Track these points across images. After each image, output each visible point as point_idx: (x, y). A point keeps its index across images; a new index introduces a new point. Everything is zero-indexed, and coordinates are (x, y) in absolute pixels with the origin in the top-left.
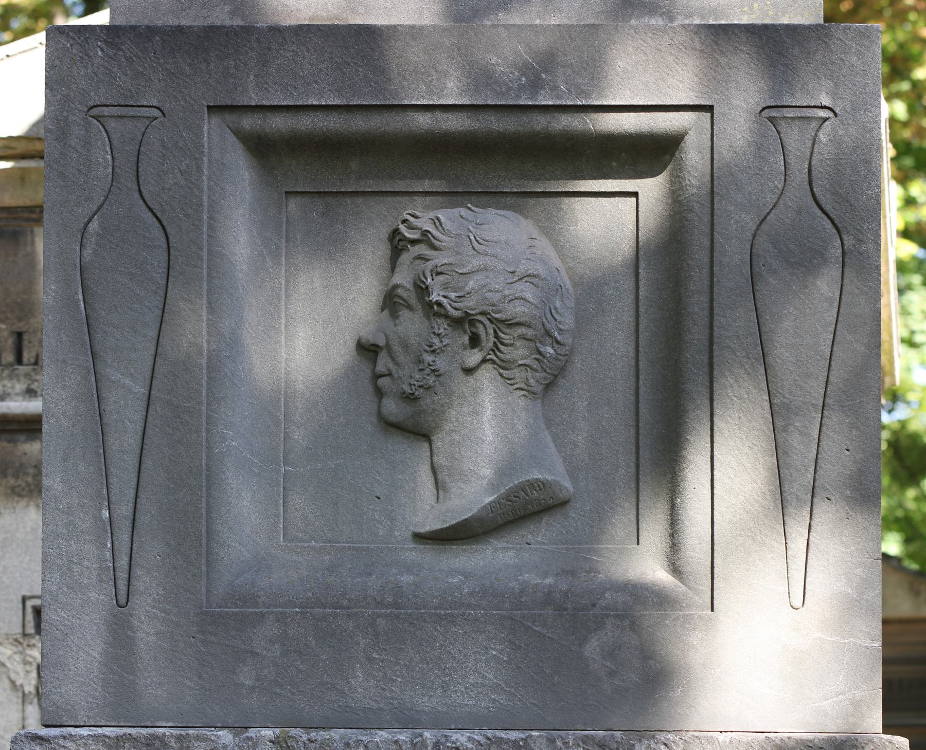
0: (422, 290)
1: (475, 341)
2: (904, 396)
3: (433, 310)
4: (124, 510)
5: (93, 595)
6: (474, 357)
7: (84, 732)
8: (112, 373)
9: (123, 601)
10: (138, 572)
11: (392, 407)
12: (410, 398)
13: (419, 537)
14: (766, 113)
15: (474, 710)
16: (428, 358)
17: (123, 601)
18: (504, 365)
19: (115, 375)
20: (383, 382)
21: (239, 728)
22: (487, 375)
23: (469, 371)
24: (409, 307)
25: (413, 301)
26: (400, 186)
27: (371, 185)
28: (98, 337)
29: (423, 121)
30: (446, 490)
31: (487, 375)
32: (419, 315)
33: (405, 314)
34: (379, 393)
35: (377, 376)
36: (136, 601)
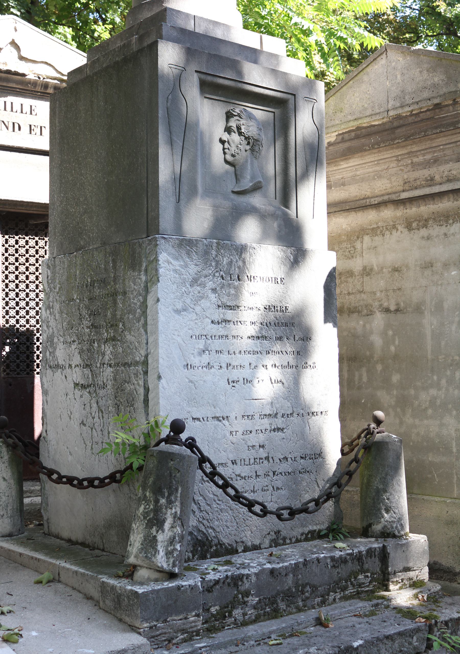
0: (239, 128)
5: (171, 199)
7: (174, 237)
8: (175, 138)
10: (181, 194)
12: (233, 156)
13: (233, 192)
14: (170, 66)
15: (57, 306)
16: (240, 146)
19: (175, 139)
20: (226, 150)
24: (235, 132)
25: (236, 130)
26: (234, 101)
27: (234, 101)
28: (171, 128)
30: (239, 181)
32: (237, 134)
33: (233, 133)
34: (225, 153)
35: (224, 149)
36: (181, 202)
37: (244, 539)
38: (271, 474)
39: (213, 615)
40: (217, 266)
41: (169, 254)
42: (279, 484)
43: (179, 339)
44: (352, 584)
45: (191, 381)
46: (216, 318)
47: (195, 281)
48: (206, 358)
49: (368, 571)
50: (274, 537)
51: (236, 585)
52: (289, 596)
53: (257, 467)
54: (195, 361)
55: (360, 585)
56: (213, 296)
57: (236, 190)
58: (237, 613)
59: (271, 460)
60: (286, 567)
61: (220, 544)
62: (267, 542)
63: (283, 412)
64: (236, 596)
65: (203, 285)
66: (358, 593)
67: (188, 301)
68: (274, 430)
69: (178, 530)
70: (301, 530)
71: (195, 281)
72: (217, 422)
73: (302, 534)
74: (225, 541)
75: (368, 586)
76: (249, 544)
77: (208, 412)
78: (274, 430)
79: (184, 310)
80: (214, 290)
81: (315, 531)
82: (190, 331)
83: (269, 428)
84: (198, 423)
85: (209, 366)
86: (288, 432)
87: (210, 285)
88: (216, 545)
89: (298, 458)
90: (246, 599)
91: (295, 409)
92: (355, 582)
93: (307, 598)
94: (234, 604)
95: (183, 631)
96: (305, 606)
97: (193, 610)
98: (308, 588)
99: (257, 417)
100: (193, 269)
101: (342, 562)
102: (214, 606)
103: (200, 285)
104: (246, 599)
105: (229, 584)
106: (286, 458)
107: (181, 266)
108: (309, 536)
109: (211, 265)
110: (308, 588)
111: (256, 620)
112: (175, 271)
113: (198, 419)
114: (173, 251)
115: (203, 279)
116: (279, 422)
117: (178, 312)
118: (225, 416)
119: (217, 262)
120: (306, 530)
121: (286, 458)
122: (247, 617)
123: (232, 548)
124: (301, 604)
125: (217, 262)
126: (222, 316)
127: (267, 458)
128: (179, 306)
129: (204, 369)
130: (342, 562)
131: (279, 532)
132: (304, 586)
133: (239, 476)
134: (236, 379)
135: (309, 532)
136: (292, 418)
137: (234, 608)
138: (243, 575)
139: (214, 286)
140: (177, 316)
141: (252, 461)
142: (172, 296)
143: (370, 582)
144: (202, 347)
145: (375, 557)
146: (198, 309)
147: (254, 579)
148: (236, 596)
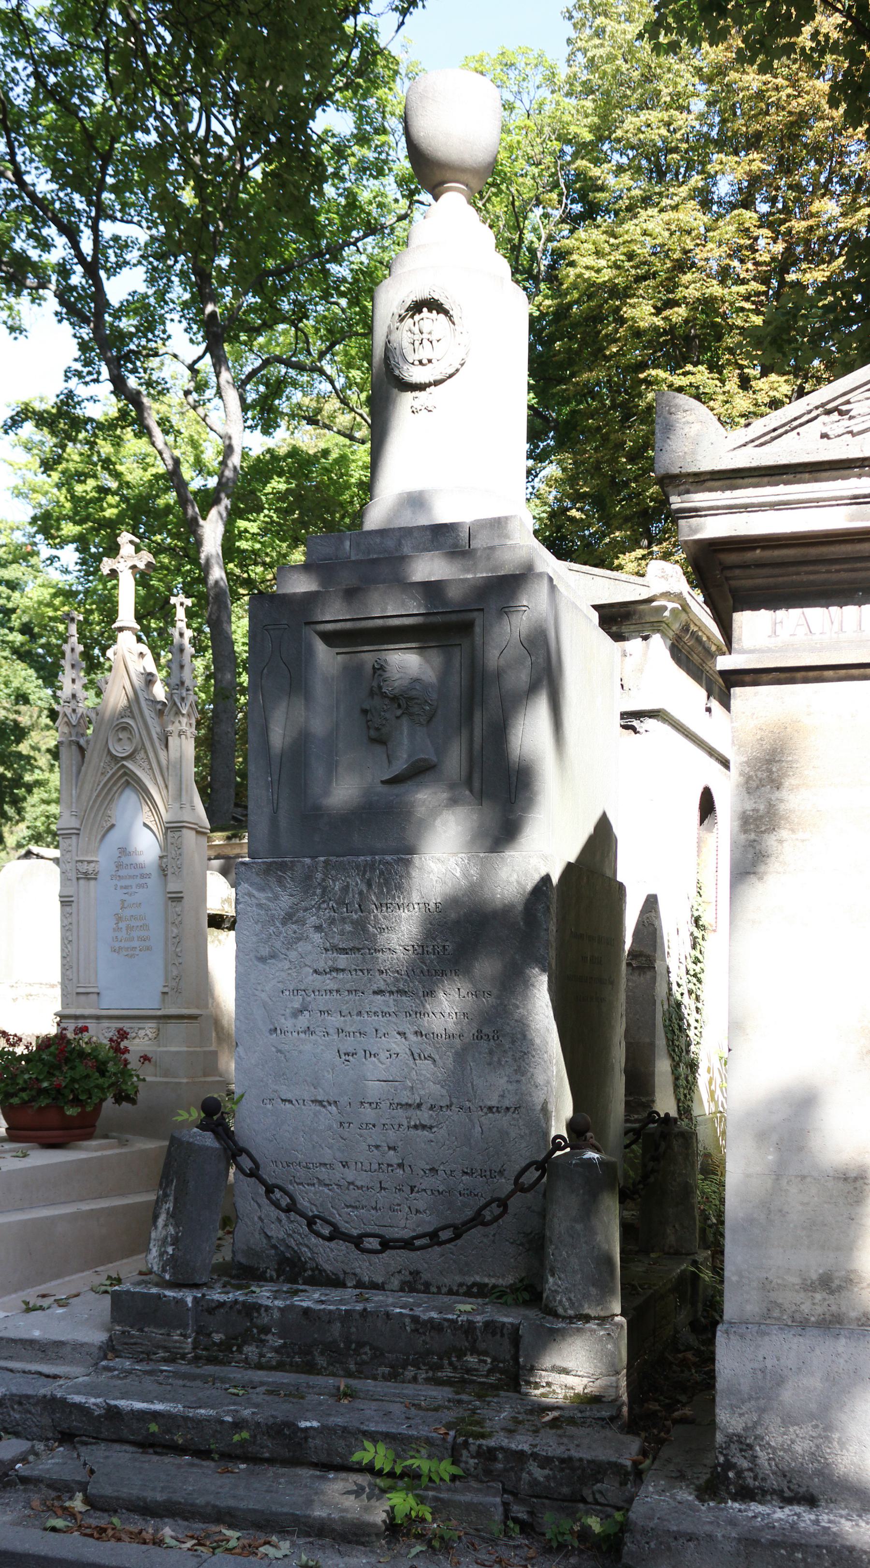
0: (380, 687)
1: (399, 706)
2: (824, 1472)
3: (384, 695)
4: (276, 777)
6: (399, 712)
9: (275, 811)
11: (372, 733)
12: (377, 729)
13: (383, 782)
17: (275, 811)
18: (411, 715)
21: (313, 857)
22: (405, 721)
23: (398, 718)
29: (379, 623)
31: (405, 721)
37: (358, 1271)
38: (407, 1189)
39: (215, 1344)
40: (323, 894)
41: (251, 885)
42: (421, 1205)
43: (263, 996)
44: (451, 1364)
45: (279, 1051)
46: (321, 965)
47: (289, 917)
48: (303, 1020)
49: (486, 1353)
50: (409, 1278)
51: (249, 1315)
52: (330, 1349)
53: (382, 1176)
54: (288, 1024)
55: (468, 1371)
56: (317, 937)
57: (386, 777)
58: (250, 1350)
59: (407, 1169)
60: (330, 1311)
61: (318, 1269)
62: (395, 1283)
63: (431, 1102)
64: (249, 1329)
65: (302, 922)
66: (463, 1381)
67: (278, 945)
68: (416, 1127)
69: (171, 1230)
70: (458, 1279)
71: (289, 917)
72: (318, 1108)
73: (461, 1285)
74: (327, 1267)
75: (487, 1376)
76: (366, 1279)
77: (307, 1093)
78: (416, 1127)
79: (273, 956)
80: (318, 928)
81: (486, 1285)
82: (280, 986)
83: (405, 1123)
84: (288, 1105)
85: (308, 1030)
86: (441, 1133)
87: (313, 920)
88: (312, 1270)
89: (458, 1173)
90: (263, 1337)
91: (454, 1100)
92: (458, 1364)
93: (364, 1363)
94: (246, 1338)
95: (166, 1349)
96: (361, 1372)
97: (178, 1327)
98: (367, 1349)
99: (384, 1105)
100: (286, 900)
101: (433, 1328)
102: (217, 1332)
103: (296, 922)
104: (263, 1337)
105: (239, 1312)
106: (434, 1170)
107: (268, 899)
108: (475, 1290)
109: (314, 894)
110: (367, 1349)
111: (280, 1367)
112: (260, 906)
113: (290, 1102)
114: (257, 880)
115: (301, 914)
116: (424, 1116)
117: (262, 959)
118: (331, 1099)
119: (324, 889)
120: (470, 1280)
121: (434, 1170)
122: (263, 1360)
123: (338, 1278)
124: (352, 1367)
125: (324, 889)
126: (330, 963)
127: (401, 1166)
128: (265, 951)
129: (302, 1035)
130: (433, 1328)
131: (418, 1273)
132: (361, 1345)
133: (352, 1183)
134: (351, 1050)
135: (474, 1284)
136: (449, 1113)
137: (245, 1342)
138: (261, 1306)
139: (318, 922)
140: (261, 966)
141: (375, 1166)
142: (254, 939)
143: (490, 1372)
144: (297, 1005)
145: (502, 1335)
146: (293, 955)
147: (276, 1315)
148: (249, 1329)
